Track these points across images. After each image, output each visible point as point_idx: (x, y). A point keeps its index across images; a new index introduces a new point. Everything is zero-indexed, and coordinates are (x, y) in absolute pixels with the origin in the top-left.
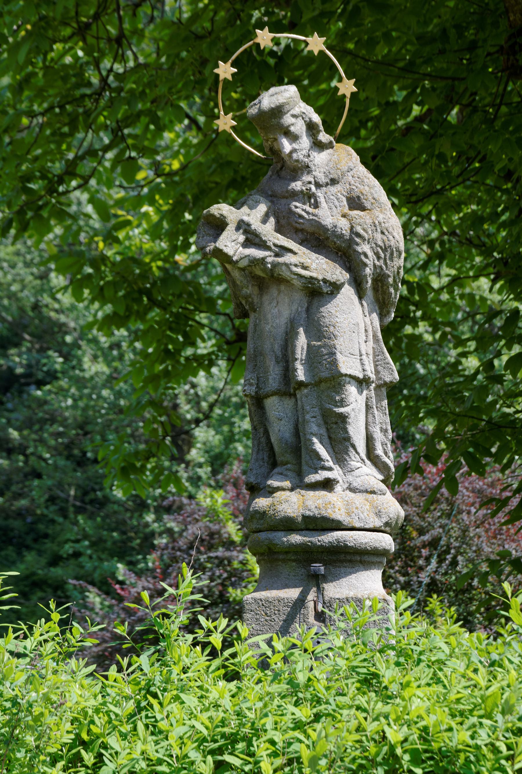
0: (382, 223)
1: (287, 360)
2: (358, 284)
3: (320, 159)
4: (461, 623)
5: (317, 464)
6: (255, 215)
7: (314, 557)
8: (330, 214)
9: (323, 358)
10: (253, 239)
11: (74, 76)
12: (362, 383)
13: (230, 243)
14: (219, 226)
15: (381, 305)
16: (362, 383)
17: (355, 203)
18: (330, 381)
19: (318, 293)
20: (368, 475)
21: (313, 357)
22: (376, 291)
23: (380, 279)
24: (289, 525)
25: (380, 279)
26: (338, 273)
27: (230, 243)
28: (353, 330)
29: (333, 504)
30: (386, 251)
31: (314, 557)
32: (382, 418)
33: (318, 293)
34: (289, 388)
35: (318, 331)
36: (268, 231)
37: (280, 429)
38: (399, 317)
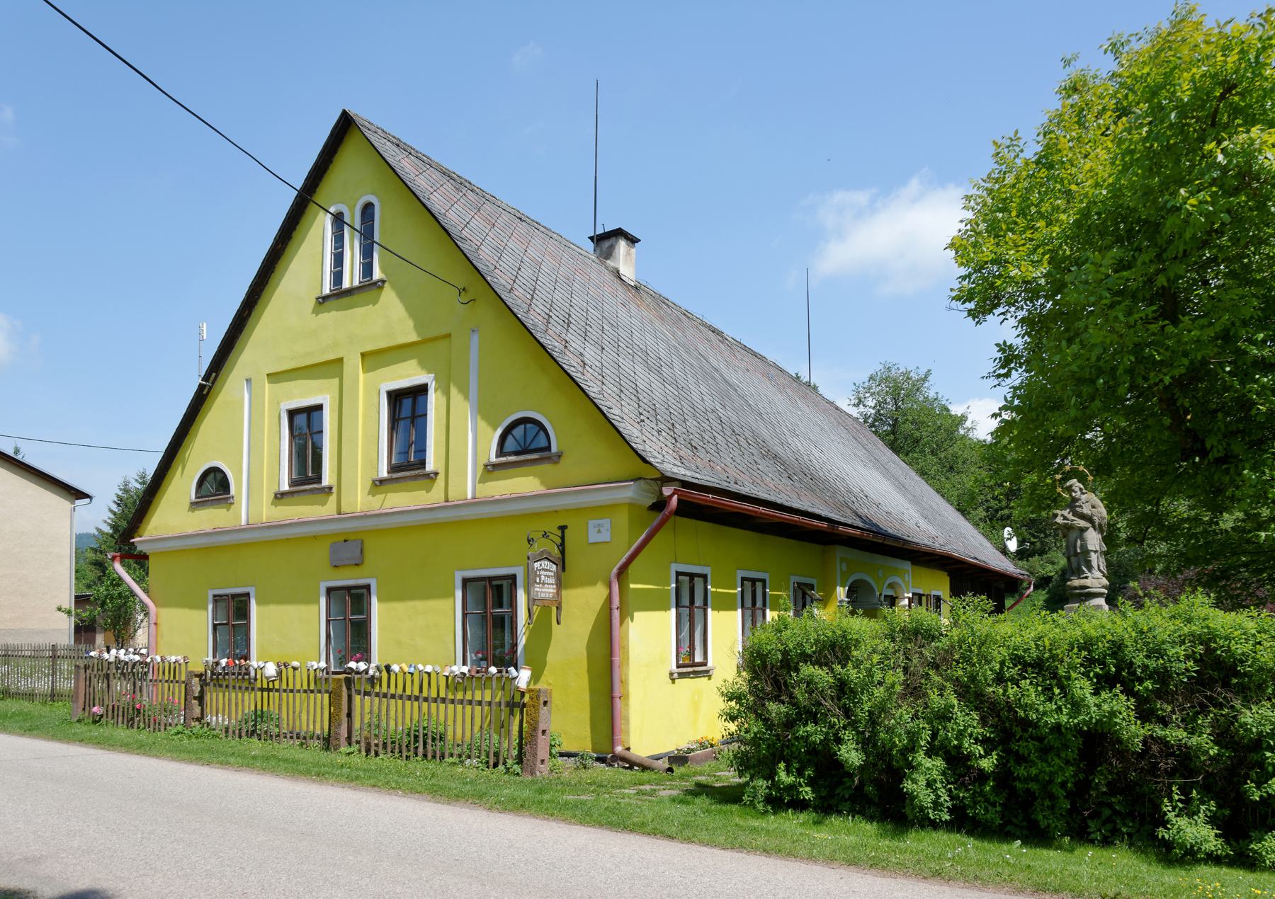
0: (1101, 512)
1: (1075, 547)
2: (1094, 527)
3: (1083, 497)
4: (971, 305)
5: (1083, 572)
6: (1066, 513)
7: (1085, 595)
8: (1086, 510)
9: (1084, 547)
10: (1065, 518)
11: (771, 775)
12: (1096, 552)
13: (1059, 520)
14: (1056, 516)
15: (1101, 531)
16: (1096, 552)
17: (1093, 507)
18: (1086, 552)
19: (1083, 530)
20: (1099, 574)
21: (1082, 547)
22: (1100, 529)
23: (1100, 525)
24: (1076, 588)
25: (1100, 525)
26: (1088, 525)
27: (1059, 520)
28: (1093, 540)
29: (1088, 582)
30: (1102, 518)
31: (1085, 595)
32: (1102, 560)
33: (1083, 530)
34: (1076, 554)
35: (1083, 540)
36: (1070, 516)
37: (1074, 565)
38: (1110, 538)
